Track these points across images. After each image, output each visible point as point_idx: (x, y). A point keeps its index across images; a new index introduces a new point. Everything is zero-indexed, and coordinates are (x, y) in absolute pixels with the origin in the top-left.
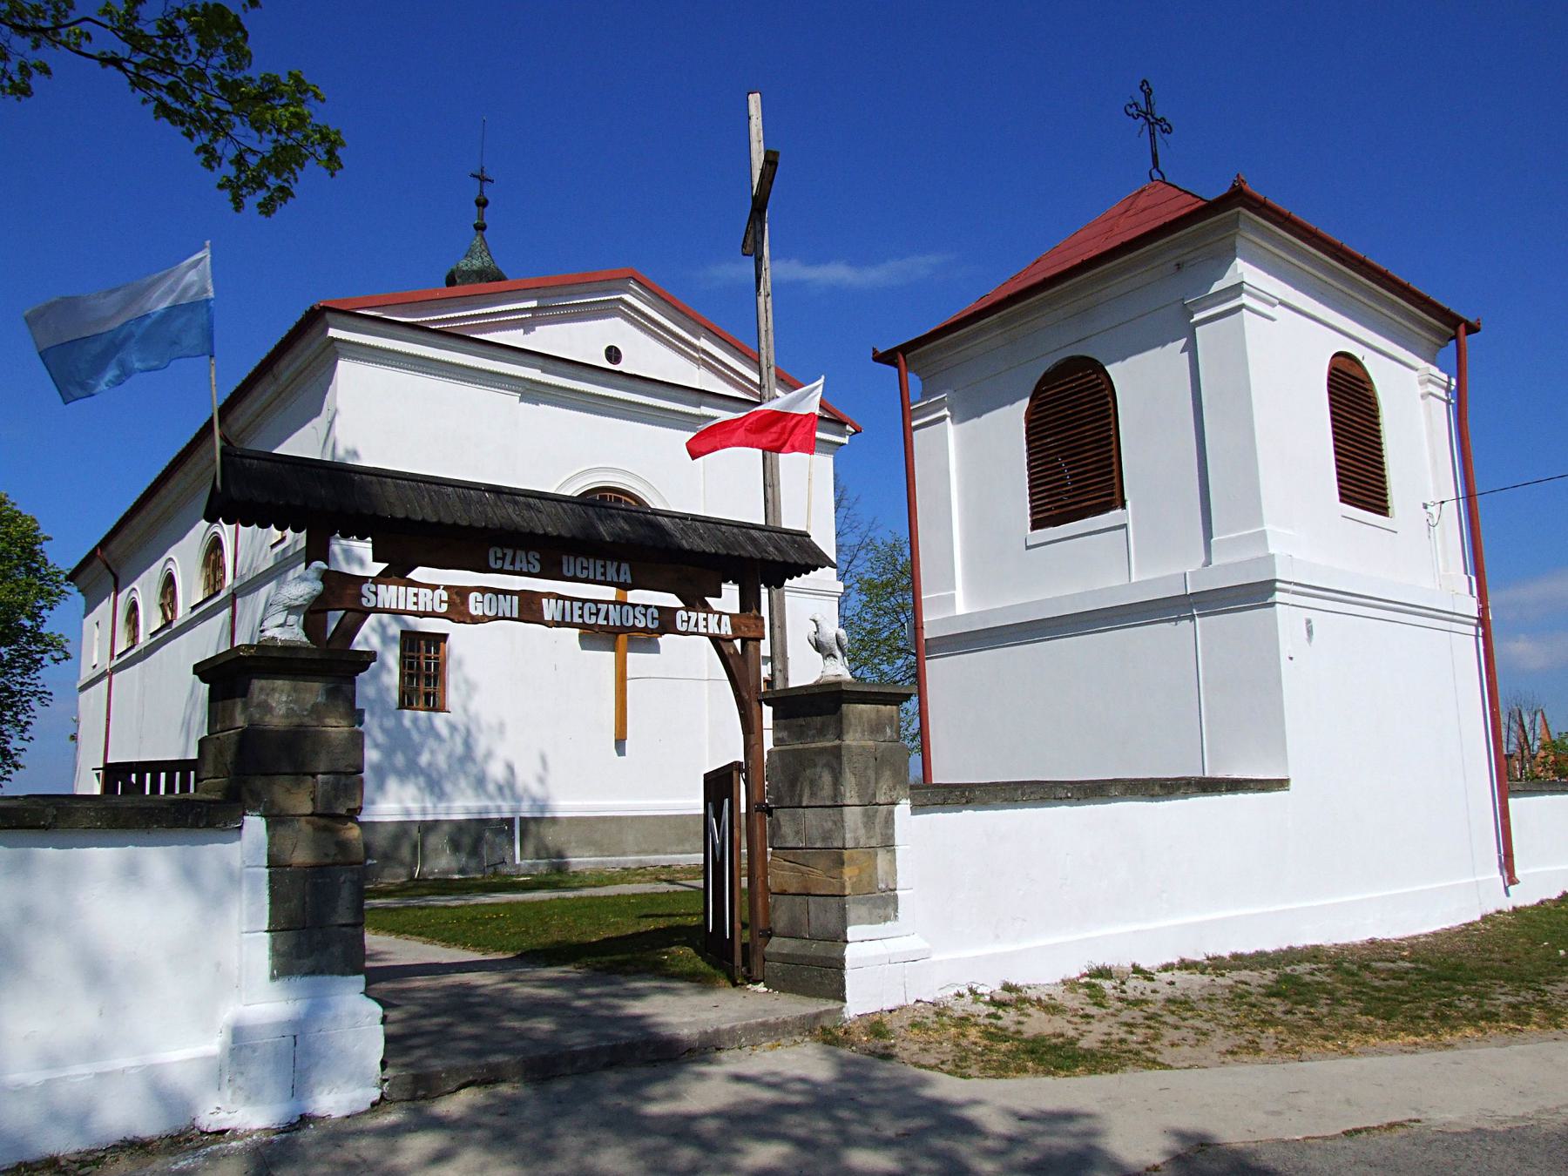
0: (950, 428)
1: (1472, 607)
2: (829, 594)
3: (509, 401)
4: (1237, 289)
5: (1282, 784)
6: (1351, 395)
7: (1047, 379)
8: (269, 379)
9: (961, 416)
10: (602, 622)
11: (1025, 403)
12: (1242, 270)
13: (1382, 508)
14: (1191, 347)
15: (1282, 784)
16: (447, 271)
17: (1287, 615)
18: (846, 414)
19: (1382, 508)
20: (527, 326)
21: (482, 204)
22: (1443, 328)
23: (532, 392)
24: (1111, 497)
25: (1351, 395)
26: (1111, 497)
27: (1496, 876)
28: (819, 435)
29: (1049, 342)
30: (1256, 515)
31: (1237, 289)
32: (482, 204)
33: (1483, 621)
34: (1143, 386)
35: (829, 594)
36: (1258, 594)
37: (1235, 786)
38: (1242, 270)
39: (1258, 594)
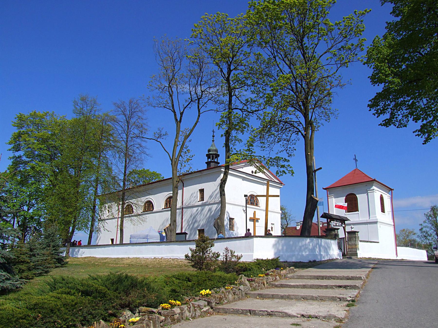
0: (334, 199)
1: (393, 224)
2: (279, 213)
3: (240, 180)
4: (373, 190)
5: (378, 242)
6: (382, 199)
7: (348, 195)
8: (200, 172)
9: (335, 198)
10: (107, 205)
11: (345, 197)
12: (374, 187)
13: (384, 212)
14: (368, 195)
15: (378, 242)
16: (208, 149)
17: (378, 225)
18: (282, 182)
19: (384, 212)
20: (242, 168)
21: (213, 136)
22: (390, 190)
23: (244, 179)
24: (357, 210)
25: (382, 199)
26: (357, 210)
27: (395, 256)
28: (270, 183)
29: (349, 191)
30: (375, 214)
31: (373, 190)
32: (213, 136)
33: (394, 225)
34: (361, 198)
35: (279, 213)
36: (376, 223)
37: (374, 242)
38: (374, 187)
39: (376, 223)
